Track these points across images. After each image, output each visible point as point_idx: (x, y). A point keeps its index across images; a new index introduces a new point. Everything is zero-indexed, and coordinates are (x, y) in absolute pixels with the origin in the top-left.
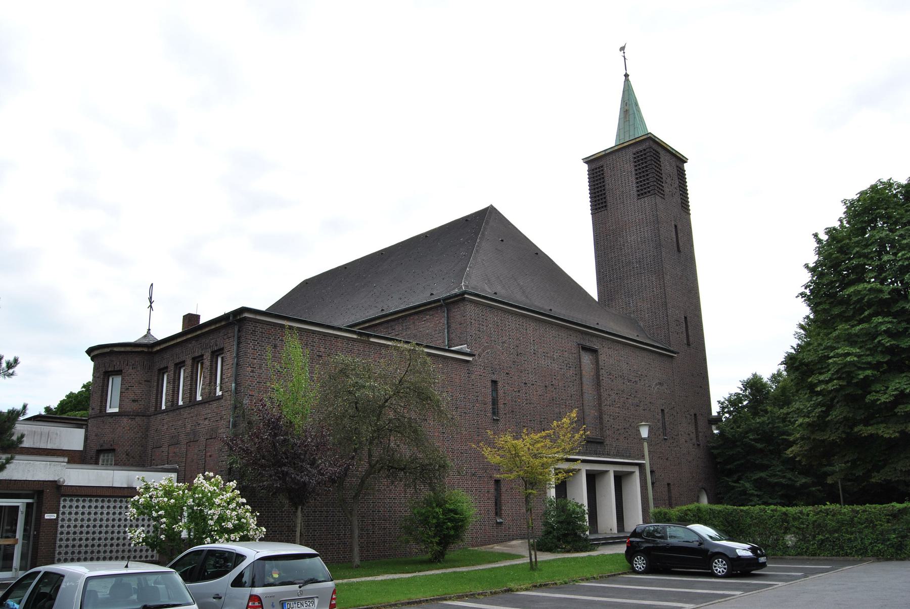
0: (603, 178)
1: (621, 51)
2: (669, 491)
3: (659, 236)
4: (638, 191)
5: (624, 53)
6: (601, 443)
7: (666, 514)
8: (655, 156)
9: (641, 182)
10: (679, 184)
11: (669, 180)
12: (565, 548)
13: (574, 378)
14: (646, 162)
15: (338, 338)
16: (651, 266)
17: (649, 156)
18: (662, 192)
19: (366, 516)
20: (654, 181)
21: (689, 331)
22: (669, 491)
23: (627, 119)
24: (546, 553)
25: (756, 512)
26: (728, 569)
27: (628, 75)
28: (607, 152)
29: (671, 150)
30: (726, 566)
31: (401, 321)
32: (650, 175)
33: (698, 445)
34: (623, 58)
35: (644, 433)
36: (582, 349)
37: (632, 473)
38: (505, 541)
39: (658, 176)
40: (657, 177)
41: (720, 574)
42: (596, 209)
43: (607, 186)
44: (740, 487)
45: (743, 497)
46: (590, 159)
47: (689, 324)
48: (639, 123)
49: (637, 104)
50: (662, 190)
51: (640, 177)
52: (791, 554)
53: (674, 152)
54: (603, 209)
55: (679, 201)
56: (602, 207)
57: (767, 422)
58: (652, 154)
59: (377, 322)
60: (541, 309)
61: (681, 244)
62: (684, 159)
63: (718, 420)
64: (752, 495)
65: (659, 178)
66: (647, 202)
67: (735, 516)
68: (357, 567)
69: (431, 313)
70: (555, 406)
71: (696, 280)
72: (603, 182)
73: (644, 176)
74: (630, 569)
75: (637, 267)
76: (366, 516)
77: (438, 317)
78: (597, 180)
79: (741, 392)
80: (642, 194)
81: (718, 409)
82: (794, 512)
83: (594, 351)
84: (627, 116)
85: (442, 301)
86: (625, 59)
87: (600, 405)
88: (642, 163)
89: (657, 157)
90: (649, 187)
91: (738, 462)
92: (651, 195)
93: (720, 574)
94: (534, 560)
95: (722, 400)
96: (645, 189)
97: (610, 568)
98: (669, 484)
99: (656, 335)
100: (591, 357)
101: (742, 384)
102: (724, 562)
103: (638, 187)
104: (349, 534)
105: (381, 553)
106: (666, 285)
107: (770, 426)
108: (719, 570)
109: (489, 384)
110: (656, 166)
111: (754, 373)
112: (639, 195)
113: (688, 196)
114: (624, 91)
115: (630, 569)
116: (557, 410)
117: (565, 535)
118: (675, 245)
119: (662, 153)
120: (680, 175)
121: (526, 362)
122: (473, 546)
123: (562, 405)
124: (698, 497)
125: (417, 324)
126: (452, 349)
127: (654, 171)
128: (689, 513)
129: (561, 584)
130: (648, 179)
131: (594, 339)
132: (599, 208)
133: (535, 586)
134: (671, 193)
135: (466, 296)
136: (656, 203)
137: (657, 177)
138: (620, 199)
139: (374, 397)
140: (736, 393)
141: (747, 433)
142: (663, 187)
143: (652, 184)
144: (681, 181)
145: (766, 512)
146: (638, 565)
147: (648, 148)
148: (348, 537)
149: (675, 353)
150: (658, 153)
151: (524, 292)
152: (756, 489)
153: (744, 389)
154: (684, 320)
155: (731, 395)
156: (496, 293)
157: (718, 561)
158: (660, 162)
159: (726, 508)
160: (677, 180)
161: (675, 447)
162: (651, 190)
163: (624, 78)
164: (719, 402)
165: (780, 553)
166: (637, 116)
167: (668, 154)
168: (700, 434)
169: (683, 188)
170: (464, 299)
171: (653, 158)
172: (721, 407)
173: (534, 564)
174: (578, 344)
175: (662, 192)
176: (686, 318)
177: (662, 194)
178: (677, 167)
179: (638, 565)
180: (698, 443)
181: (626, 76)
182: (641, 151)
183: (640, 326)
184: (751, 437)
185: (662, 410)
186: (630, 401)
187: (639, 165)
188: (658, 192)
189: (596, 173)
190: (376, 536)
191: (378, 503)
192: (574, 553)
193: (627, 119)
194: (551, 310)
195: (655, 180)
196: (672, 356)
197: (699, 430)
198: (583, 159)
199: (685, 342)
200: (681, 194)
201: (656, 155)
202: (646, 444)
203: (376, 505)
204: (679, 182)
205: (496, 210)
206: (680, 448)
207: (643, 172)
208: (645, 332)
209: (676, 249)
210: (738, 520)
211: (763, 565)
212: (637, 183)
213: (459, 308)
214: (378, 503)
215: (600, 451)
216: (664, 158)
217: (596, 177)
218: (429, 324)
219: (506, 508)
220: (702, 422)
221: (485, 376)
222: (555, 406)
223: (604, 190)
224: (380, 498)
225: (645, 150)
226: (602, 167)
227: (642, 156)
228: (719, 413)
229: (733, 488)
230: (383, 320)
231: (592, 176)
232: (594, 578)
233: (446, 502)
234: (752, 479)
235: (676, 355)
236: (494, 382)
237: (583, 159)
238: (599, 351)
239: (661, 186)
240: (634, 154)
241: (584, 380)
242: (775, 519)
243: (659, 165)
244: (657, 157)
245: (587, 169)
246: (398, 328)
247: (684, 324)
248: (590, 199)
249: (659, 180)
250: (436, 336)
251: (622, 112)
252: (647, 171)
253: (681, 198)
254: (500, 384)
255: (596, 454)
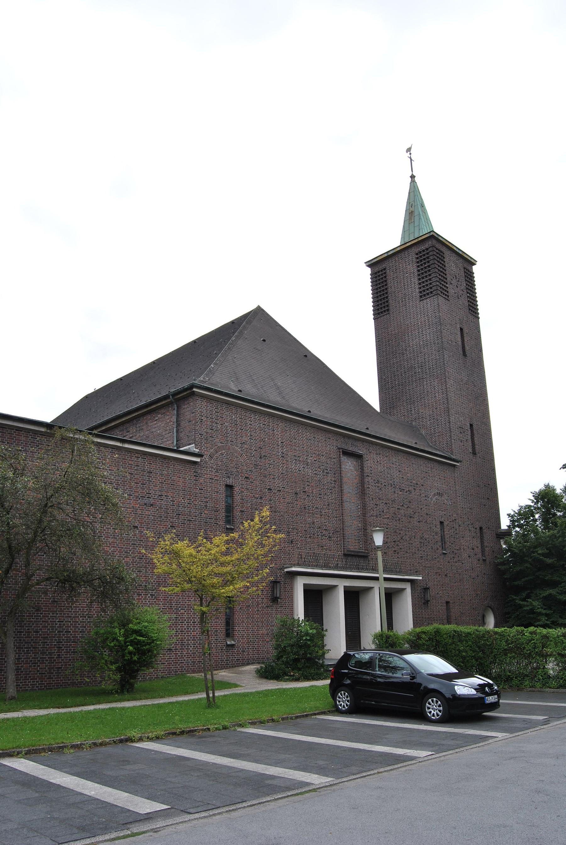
0: (386, 281)
1: (407, 152)
2: (448, 609)
3: (442, 338)
4: (420, 292)
5: (410, 154)
6: (365, 557)
7: (389, 638)
8: (438, 255)
9: (423, 282)
10: (466, 287)
11: (454, 282)
12: (293, 675)
13: (333, 485)
14: (428, 262)
15: (22, 431)
16: (433, 370)
17: (431, 255)
18: (446, 293)
19: (50, 637)
20: (437, 281)
21: (476, 439)
22: (448, 609)
23: (412, 221)
24: (272, 681)
25: (512, 635)
26: (444, 712)
27: (414, 177)
28: (389, 254)
29: (458, 251)
30: (441, 708)
31: (135, 422)
32: (433, 275)
33: (484, 560)
34: (410, 159)
35: (378, 539)
36: (343, 453)
37: (403, 590)
38: (238, 666)
39: (442, 276)
40: (440, 277)
41: (434, 718)
42: (379, 314)
43: (389, 290)
44: (528, 606)
45: (532, 616)
46: (372, 262)
47: (475, 432)
48: (424, 224)
49: (423, 206)
50: (445, 291)
51: (423, 278)
52: (552, 686)
53: (460, 253)
54: (385, 314)
55: (467, 304)
56: (385, 311)
57: (557, 535)
58: (435, 253)
59: (113, 424)
60: (296, 409)
61: (467, 348)
62: (473, 261)
63: (508, 533)
64: (540, 614)
65: (442, 278)
66: (430, 304)
67: (487, 639)
68: (11, 699)
69: (163, 411)
70: (307, 515)
71: (485, 386)
72: (386, 285)
73: (426, 277)
74: (333, 707)
75: (419, 372)
76: (50, 637)
77: (168, 415)
78: (379, 284)
79: (532, 504)
80: (425, 295)
81: (508, 523)
82: (555, 636)
83: (358, 457)
84: (412, 218)
85: (171, 397)
86: (411, 160)
87: (364, 515)
88: (425, 263)
89: (440, 257)
90: (431, 288)
91: (526, 579)
92: (434, 296)
93: (434, 718)
94: (211, 695)
95: (512, 513)
96: (428, 289)
97: (308, 706)
98: (447, 603)
99: (438, 442)
100: (355, 463)
101: (534, 496)
102: (439, 702)
103: (420, 288)
104: (24, 658)
105: (69, 680)
106: (448, 389)
107: (560, 539)
108: (433, 712)
109: (222, 489)
110: (439, 266)
111: (547, 484)
112: (421, 297)
113: (477, 299)
114: (409, 193)
115: (333, 707)
116: (309, 520)
117: (296, 660)
118: (460, 349)
119: (447, 253)
120: (468, 278)
121: (272, 466)
122: (194, 672)
123: (317, 514)
124: (484, 617)
125: (150, 424)
126: (181, 449)
127: (437, 270)
128: (423, 636)
129: (217, 729)
130: (430, 279)
131: (359, 444)
132: (382, 312)
133: (174, 734)
134: (456, 294)
135: (194, 390)
136: (438, 304)
137: (440, 277)
138: (402, 302)
139: (531, 564)
140: (526, 506)
141: (535, 547)
142: (447, 288)
143: (434, 284)
144: (469, 283)
145: (524, 634)
146: (341, 702)
147: (431, 247)
148: (23, 661)
149: (457, 462)
150: (441, 252)
151: (280, 393)
152: (545, 607)
153: (535, 501)
154: (469, 427)
155: (521, 507)
156: (240, 391)
157: (433, 701)
158: (444, 262)
159: (477, 630)
160: (465, 282)
161: (456, 562)
162: (434, 291)
163: (410, 179)
164: (509, 515)
165: (538, 685)
166: (422, 217)
167: (454, 254)
168: (487, 549)
169: (471, 291)
170: (193, 393)
171: (436, 258)
172: (511, 521)
173: (211, 700)
174: (339, 449)
175: (446, 293)
176: (471, 425)
177: (446, 295)
178: (465, 268)
179: (341, 702)
180: (484, 558)
181: (413, 177)
182: (424, 251)
183: (421, 434)
184: (540, 552)
185: (442, 523)
186: (402, 512)
187: (422, 265)
188: (441, 292)
189: (379, 276)
190: (63, 660)
191: (66, 622)
192: (304, 681)
193: (412, 221)
194: (309, 411)
195: (438, 279)
196: (454, 466)
197: (486, 544)
198: (365, 263)
199: (471, 450)
200: (468, 297)
201: (440, 255)
202: (379, 554)
203: (64, 625)
204: (467, 284)
205: (264, 311)
206: (462, 563)
207: (426, 272)
208: (426, 441)
209: (462, 353)
210: (490, 645)
211: (494, 706)
212: (420, 284)
213: (189, 403)
214: (66, 622)
215: (363, 566)
216: (450, 260)
217: (379, 280)
218: (160, 423)
219: (239, 629)
220: (489, 536)
221: (218, 480)
222: (307, 515)
223: (387, 293)
224: (70, 617)
225: (427, 249)
226: (385, 269)
227: (424, 255)
228: (509, 526)
229: (521, 606)
230: (118, 422)
231: (375, 279)
232: (273, 720)
233: (130, 621)
234: (541, 596)
235: (458, 464)
236: (230, 487)
237: (365, 263)
238: (365, 456)
239: (445, 286)
240: (417, 254)
241: (345, 487)
242: (534, 643)
243: (443, 265)
244: (440, 257)
245: (370, 273)
246: (132, 429)
247: (470, 432)
248: (372, 304)
249: (442, 281)
250: (166, 436)
251: (408, 214)
252: (429, 271)
253: (468, 301)
254: (237, 489)
255: (358, 569)
